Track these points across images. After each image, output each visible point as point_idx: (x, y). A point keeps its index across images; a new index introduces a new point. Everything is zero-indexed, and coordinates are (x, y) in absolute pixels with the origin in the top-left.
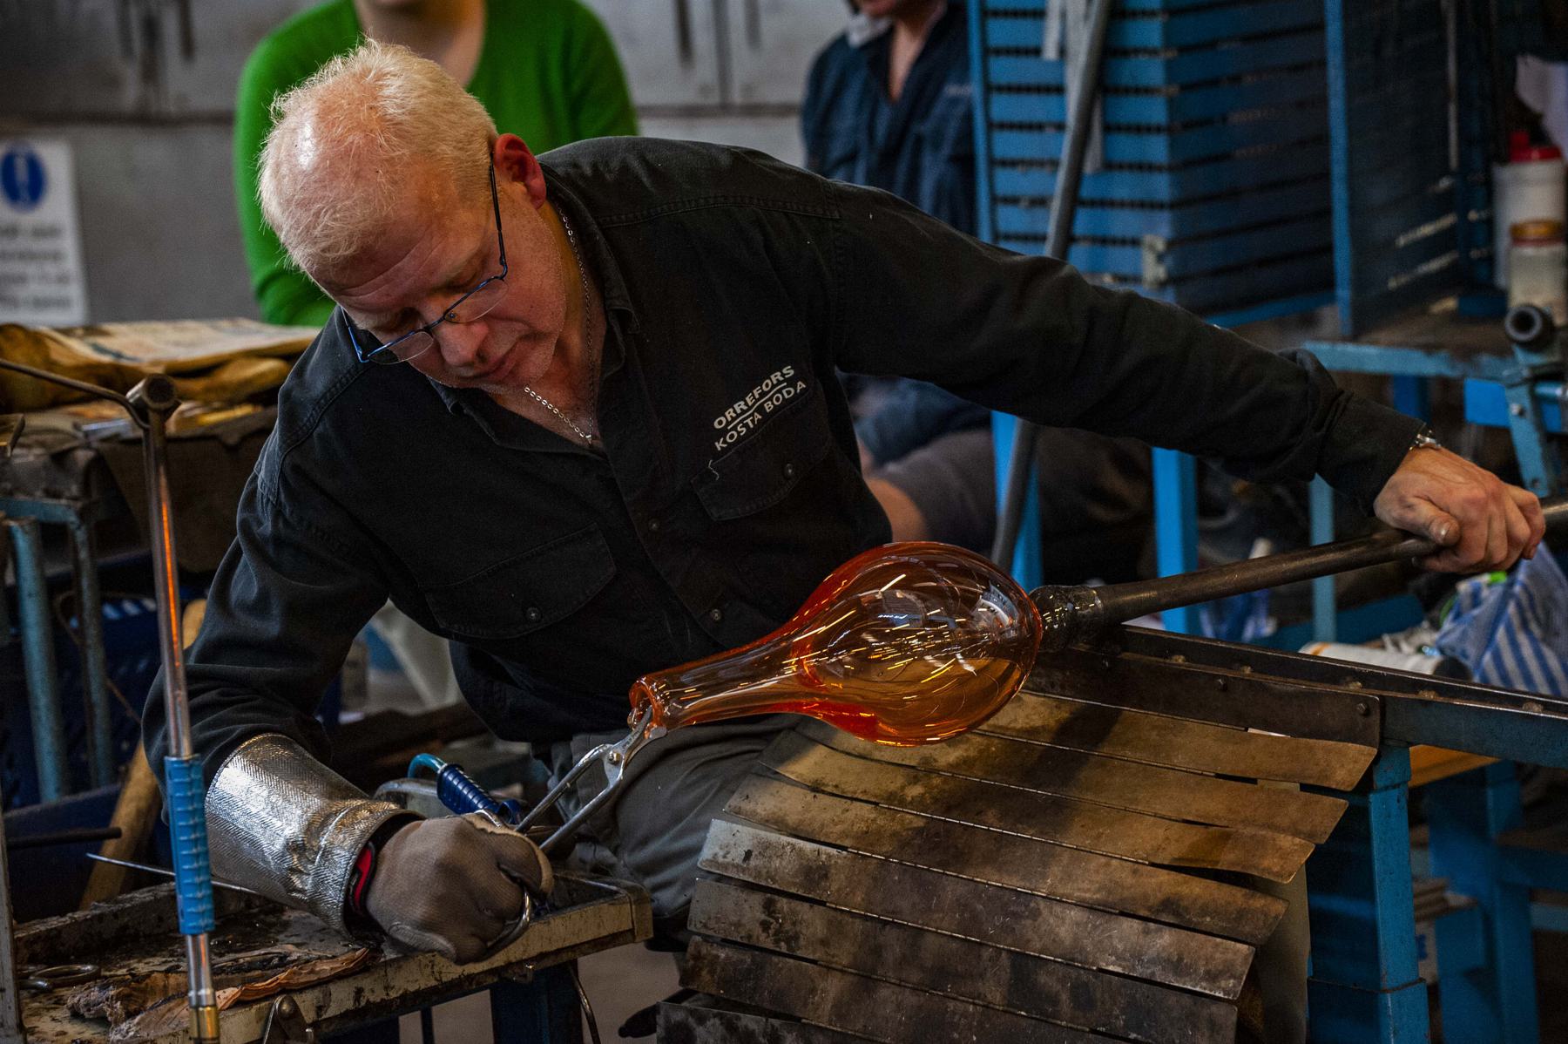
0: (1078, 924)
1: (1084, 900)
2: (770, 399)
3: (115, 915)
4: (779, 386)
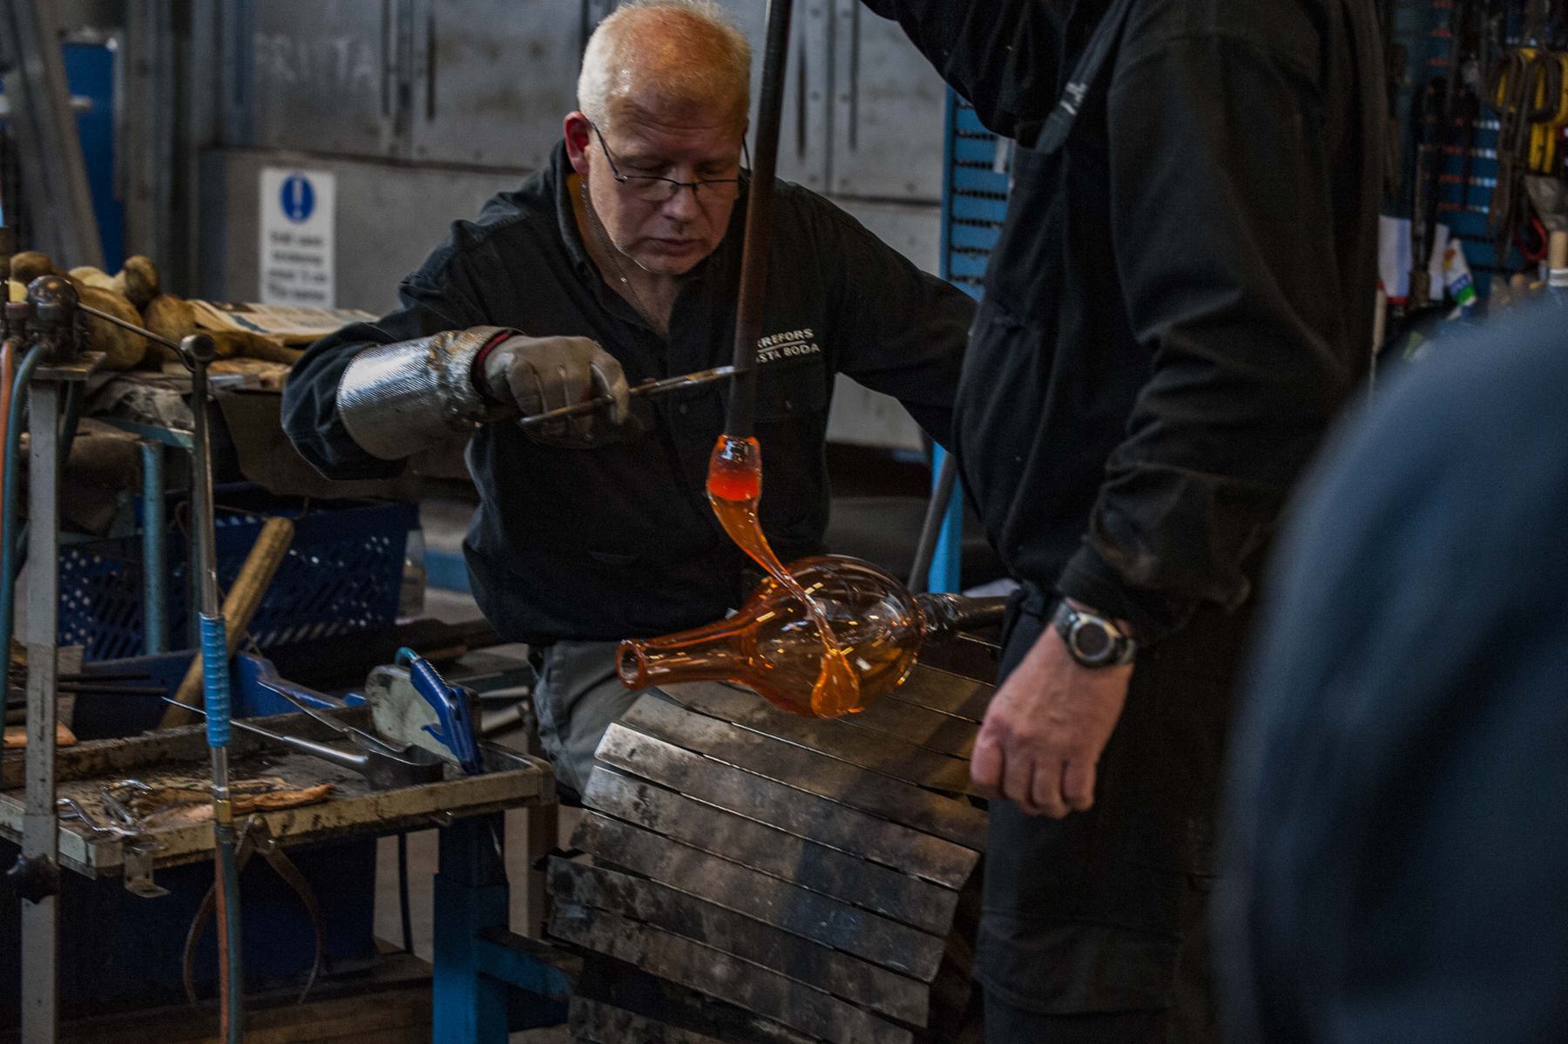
3: (158, 743)
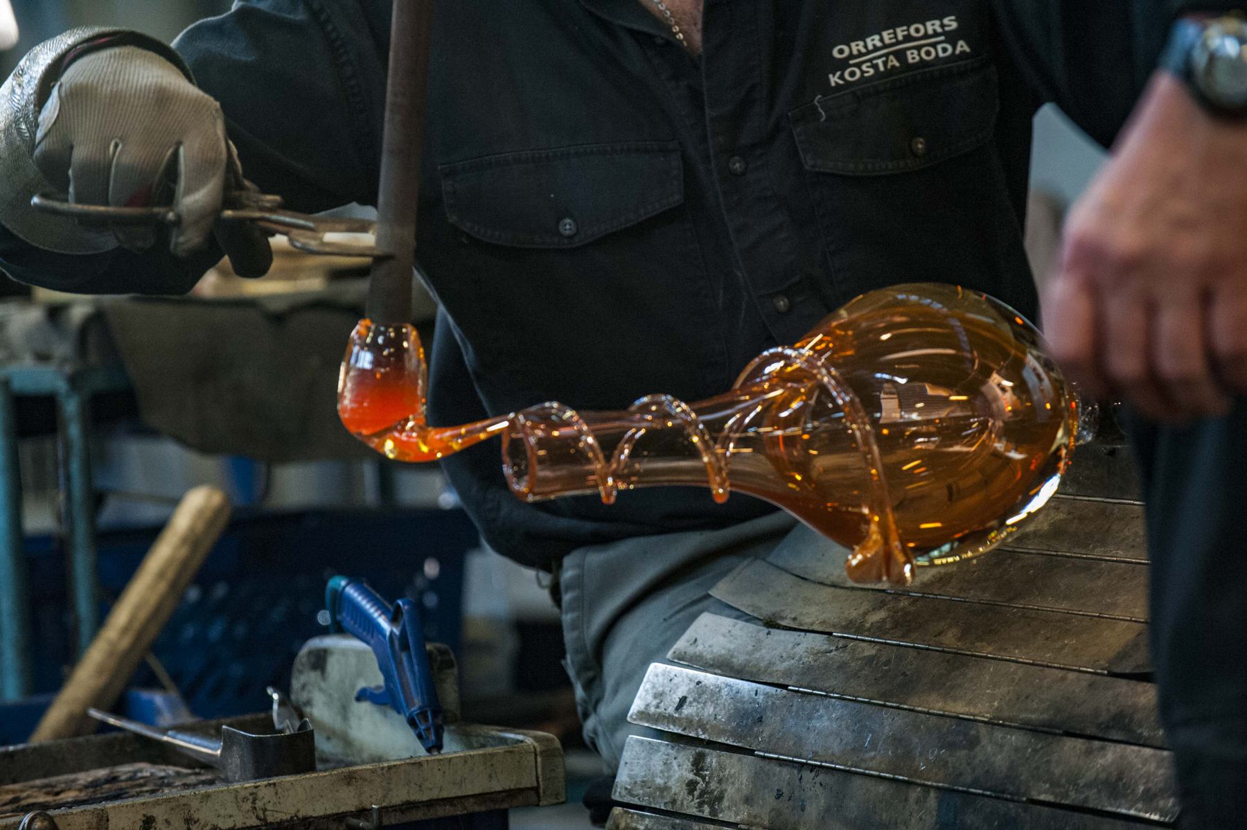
0: (1016, 750)
1: (1027, 722)
2: (919, 48)
4: (933, 39)
